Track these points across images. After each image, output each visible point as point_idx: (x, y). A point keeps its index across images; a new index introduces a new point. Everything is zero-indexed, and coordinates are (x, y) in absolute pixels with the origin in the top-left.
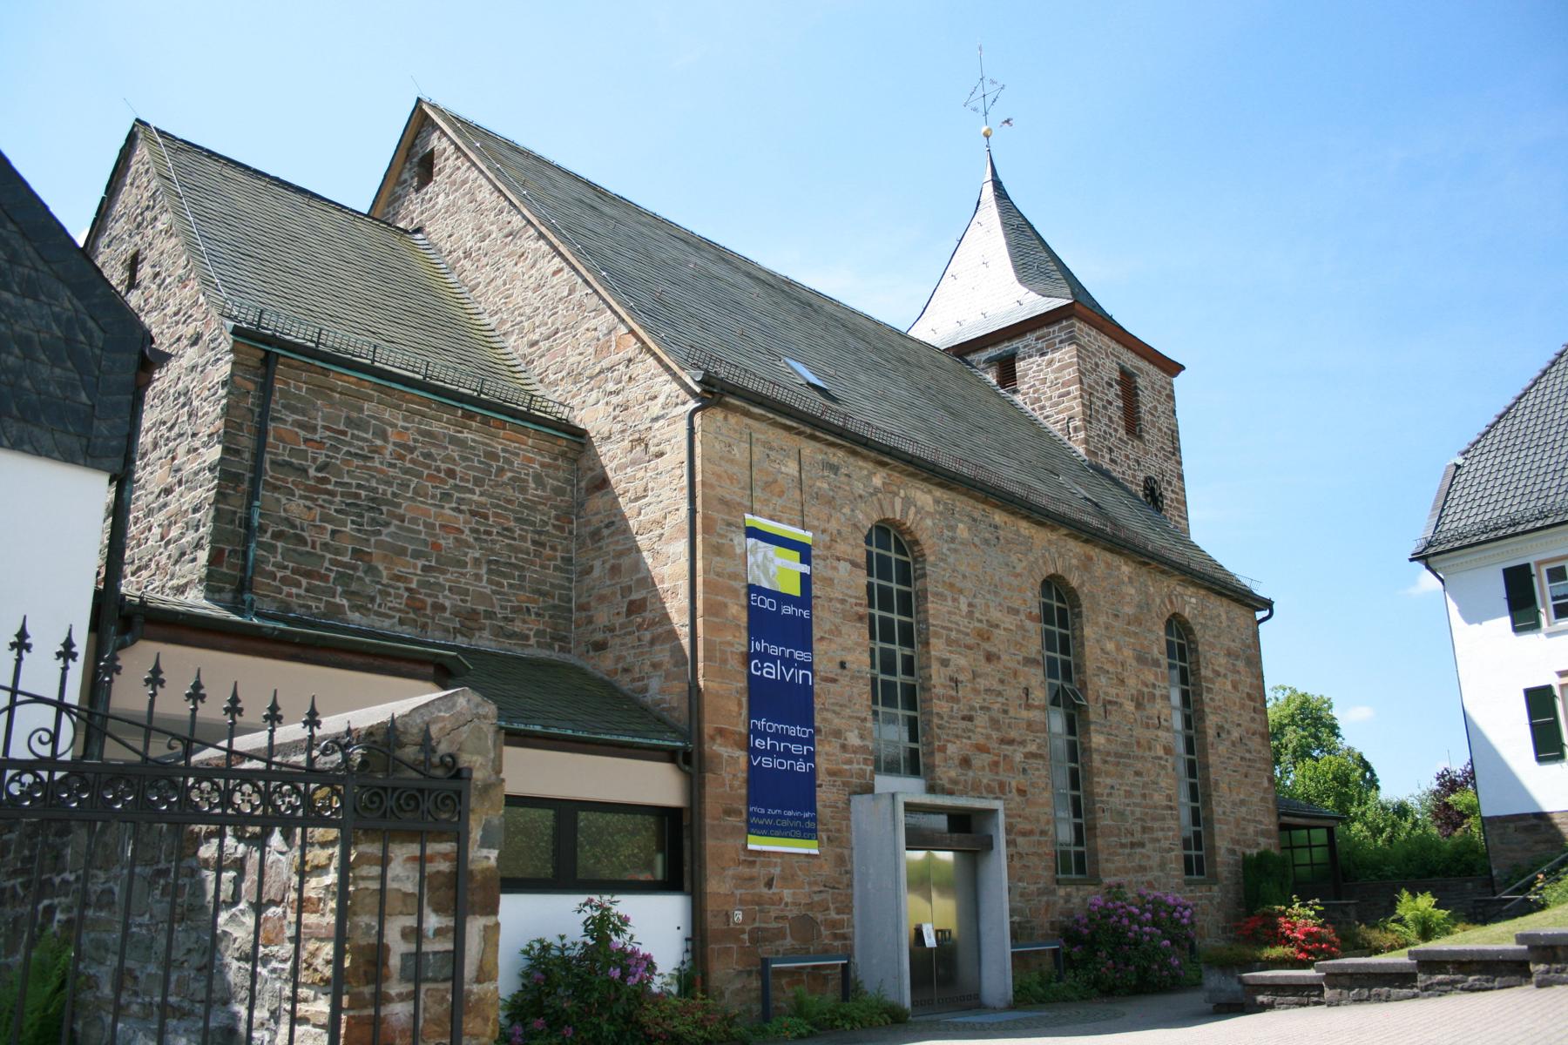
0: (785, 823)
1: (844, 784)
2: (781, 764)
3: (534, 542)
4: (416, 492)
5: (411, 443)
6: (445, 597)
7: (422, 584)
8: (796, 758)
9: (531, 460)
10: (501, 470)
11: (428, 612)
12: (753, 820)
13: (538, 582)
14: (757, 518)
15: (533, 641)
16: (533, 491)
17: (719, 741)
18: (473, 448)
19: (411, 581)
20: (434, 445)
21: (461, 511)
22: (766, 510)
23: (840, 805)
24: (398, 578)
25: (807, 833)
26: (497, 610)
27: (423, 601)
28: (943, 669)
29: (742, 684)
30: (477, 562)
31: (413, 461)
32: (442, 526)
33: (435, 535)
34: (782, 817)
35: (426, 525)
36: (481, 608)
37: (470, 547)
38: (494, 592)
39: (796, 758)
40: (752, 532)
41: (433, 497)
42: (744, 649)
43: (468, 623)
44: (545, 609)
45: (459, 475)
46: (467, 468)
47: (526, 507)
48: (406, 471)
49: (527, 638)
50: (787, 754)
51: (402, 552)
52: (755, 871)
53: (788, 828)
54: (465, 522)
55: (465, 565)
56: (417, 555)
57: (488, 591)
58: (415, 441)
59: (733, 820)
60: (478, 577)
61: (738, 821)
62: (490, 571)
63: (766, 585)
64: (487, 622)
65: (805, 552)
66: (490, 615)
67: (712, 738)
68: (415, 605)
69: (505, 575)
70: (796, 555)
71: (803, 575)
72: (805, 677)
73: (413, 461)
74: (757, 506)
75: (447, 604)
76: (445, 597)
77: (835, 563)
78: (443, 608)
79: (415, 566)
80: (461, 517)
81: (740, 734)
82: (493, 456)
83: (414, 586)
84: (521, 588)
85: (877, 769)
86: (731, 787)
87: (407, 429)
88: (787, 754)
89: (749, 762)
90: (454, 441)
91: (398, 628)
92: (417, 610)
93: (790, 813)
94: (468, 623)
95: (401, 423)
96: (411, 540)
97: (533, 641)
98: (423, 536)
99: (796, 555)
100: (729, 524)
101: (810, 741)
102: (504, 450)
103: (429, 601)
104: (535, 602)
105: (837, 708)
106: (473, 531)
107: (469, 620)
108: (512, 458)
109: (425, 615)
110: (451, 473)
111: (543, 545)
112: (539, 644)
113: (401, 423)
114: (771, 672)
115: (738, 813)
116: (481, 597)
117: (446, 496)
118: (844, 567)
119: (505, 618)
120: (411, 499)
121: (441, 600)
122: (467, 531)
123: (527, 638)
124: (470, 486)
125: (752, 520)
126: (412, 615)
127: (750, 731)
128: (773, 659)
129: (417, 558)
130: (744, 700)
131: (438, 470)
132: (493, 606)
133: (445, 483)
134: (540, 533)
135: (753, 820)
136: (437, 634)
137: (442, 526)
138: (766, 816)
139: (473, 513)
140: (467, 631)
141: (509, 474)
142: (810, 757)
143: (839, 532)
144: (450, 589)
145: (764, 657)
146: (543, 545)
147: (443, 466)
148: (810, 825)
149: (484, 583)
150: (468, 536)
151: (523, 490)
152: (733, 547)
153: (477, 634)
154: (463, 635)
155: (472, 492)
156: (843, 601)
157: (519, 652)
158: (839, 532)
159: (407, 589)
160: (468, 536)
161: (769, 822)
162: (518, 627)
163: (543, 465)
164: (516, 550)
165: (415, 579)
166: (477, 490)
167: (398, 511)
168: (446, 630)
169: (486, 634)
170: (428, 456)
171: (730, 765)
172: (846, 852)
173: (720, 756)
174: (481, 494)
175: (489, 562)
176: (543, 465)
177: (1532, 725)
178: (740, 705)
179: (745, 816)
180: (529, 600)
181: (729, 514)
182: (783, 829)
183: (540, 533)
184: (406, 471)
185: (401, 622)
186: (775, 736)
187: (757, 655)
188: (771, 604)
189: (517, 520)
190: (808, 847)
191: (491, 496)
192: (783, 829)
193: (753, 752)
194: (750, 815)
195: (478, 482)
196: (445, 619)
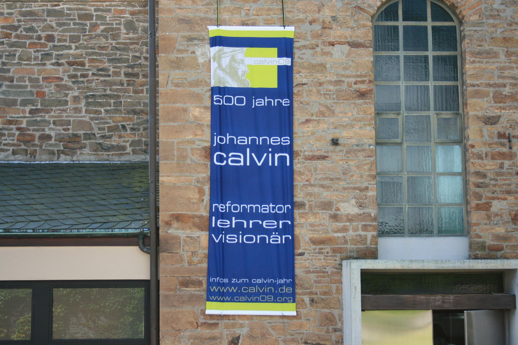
0: (254, 290)
1: (334, 251)
2: (251, 239)
3: (127, 75)
4: (20, 59)
5: (16, 24)
6: (51, 129)
7: (29, 123)
8: (269, 232)
9: (122, 12)
10: (94, 26)
11: (36, 142)
12: (214, 289)
13: (132, 104)
14: (222, 28)
15: (129, 150)
16: (124, 35)
17: (175, 224)
18: (69, 15)
19: (21, 122)
20: (34, 20)
21: (59, 64)
22: (237, 17)
23: (329, 270)
24: (10, 122)
25: (290, 297)
26: (96, 131)
27: (31, 135)
28: (487, 129)
29: (205, 174)
30: (76, 99)
31: (17, 36)
32: (44, 78)
33: (39, 86)
34: (250, 284)
35: (30, 80)
36: (82, 132)
37: (70, 89)
38: (92, 119)
39: (269, 232)
40: (217, 41)
41: (36, 58)
42: (208, 144)
43: (71, 145)
44: (139, 124)
45: (57, 38)
46: (64, 31)
47: (117, 49)
48: (12, 45)
49: (124, 148)
50: (258, 229)
51: (14, 103)
52: (216, 332)
53: (258, 294)
54: (65, 71)
55: (66, 102)
56: (25, 103)
57: (87, 119)
58: (19, 21)
59: (191, 290)
60: (77, 110)
61: (201, 291)
62: (88, 104)
63: (232, 84)
64: (87, 142)
65: (285, 47)
66: (89, 136)
67: (168, 224)
68: (25, 138)
69: (101, 105)
70: (274, 51)
71: (280, 68)
72: (282, 159)
73: (17, 36)
74: (225, 16)
75: (53, 134)
76: (51, 129)
77: (329, 49)
78: (49, 137)
79: (24, 112)
80: (61, 68)
81: (201, 217)
82: (89, 17)
83: (24, 125)
84: (117, 111)
85: (382, 233)
86: (190, 264)
87: (11, 14)
88: (258, 229)
89: (211, 240)
90: (50, 13)
91: (12, 158)
92: (26, 142)
93: (259, 281)
94: (71, 145)
95: (6, 11)
96: (19, 94)
97: (129, 150)
98: (29, 89)
99: (274, 51)
100: (190, 39)
101: (290, 215)
102: (96, 10)
103: (37, 134)
104: (130, 119)
105: (326, 183)
106: (70, 77)
107: (72, 143)
108: (104, 14)
109: (35, 145)
110: (50, 38)
111: (136, 75)
112: (134, 152)
113: (6, 11)
114: (237, 160)
115: (200, 283)
116: (81, 124)
117: (48, 56)
118: (339, 53)
119: (103, 137)
120: (19, 64)
121: (47, 132)
122: (66, 78)
123: (124, 148)
124: (67, 44)
125: (214, 31)
126: (23, 147)
127: (211, 214)
128: (242, 149)
129: (25, 105)
130: (207, 188)
131: (39, 38)
132: (92, 129)
133: (46, 46)
134: (132, 67)
135: (214, 289)
136: (44, 157)
137: (44, 78)
138: (230, 284)
139: (70, 64)
140: (69, 150)
141: (102, 27)
142: (289, 229)
143: (334, 19)
144: (54, 123)
145: (233, 147)
146: (136, 75)
147: (43, 34)
148: (287, 290)
149: (83, 113)
150: (67, 81)
151: (115, 37)
152: (196, 58)
153: (79, 152)
154: (66, 154)
155: (70, 48)
156: (338, 83)
157: (116, 160)
158: (334, 19)
159: (18, 129)
160: (67, 81)
161: (234, 289)
162: (115, 141)
163: (132, 13)
164: (111, 84)
165: (25, 120)
166: (73, 46)
167: (7, 75)
168: (52, 153)
169: (87, 151)
170: (31, 29)
171: (190, 246)
172: (336, 312)
173: (177, 238)
174: (77, 48)
175: (87, 97)
176: (132, 13)
177: (362, 296)
178: (201, 191)
179: (205, 286)
180: (124, 119)
181: (191, 30)
182: (249, 295)
183: (132, 67)
184: (12, 45)
185: (14, 153)
186: (238, 216)
187: (221, 148)
188: (240, 101)
189: (110, 61)
190: (288, 310)
191: (86, 48)
192: (249, 295)
193: (215, 231)
194: (209, 284)
195: (74, 39)
196: (51, 145)
